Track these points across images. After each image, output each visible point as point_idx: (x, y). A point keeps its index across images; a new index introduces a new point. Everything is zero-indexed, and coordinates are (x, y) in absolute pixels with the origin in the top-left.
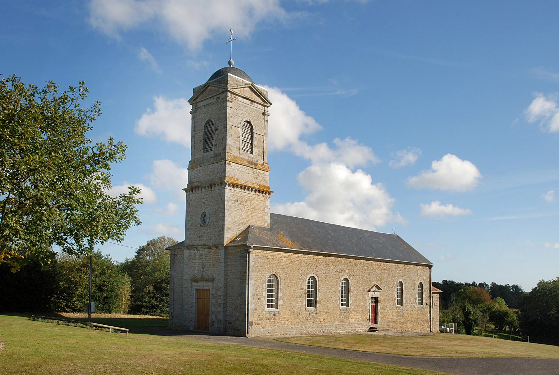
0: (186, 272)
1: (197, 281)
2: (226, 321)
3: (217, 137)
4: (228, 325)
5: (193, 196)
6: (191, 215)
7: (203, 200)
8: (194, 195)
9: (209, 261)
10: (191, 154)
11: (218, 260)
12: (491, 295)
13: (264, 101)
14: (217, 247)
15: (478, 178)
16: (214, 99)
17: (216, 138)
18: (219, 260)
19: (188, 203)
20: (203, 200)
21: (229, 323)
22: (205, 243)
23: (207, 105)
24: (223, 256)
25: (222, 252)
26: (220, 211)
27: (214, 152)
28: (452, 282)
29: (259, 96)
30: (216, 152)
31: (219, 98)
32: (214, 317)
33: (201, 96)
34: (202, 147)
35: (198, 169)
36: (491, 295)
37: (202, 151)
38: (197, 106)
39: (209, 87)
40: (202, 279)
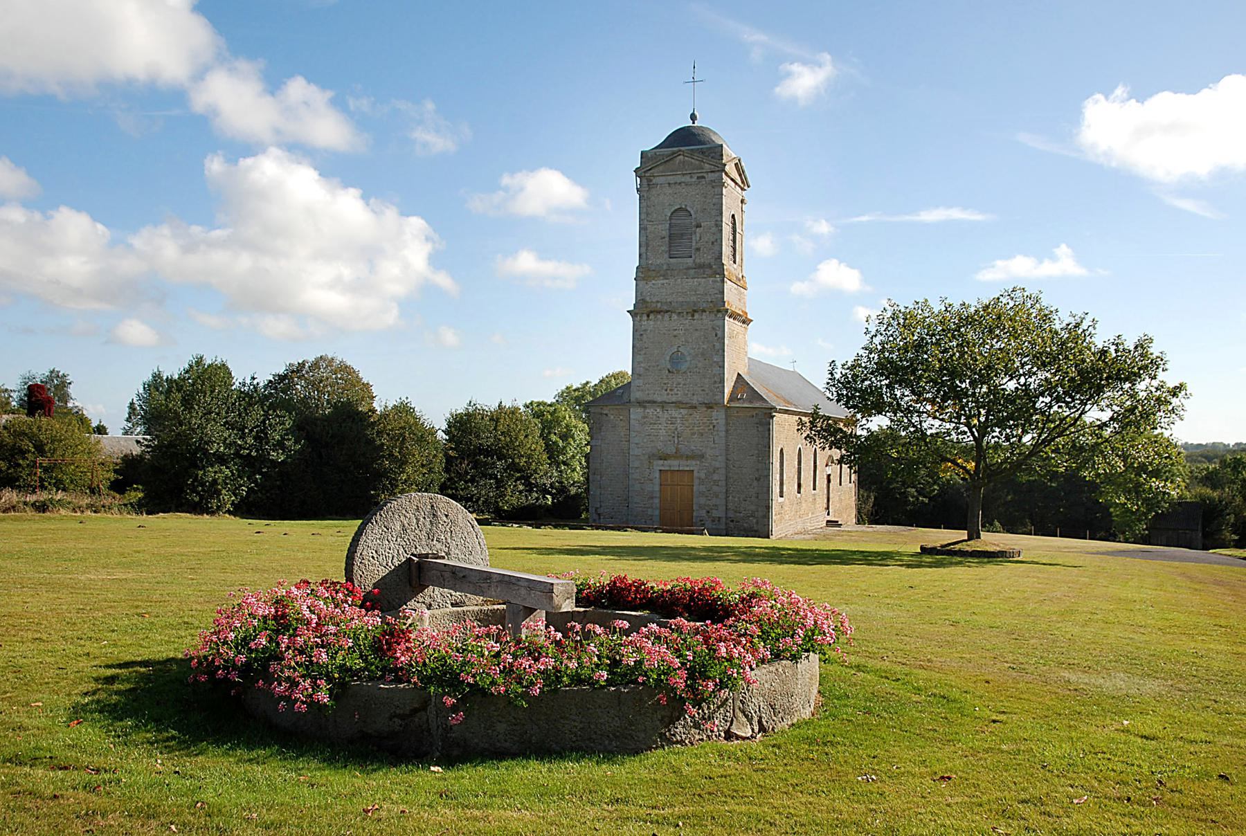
0: (637, 444)
1: (664, 457)
2: (727, 518)
3: (700, 238)
4: (732, 525)
5: (649, 324)
6: (645, 354)
7: (675, 333)
8: (651, 323)
9: (691, 428)
10: (640, 255)
11: (711, 427)
12: (1057, 251)
13: (743, 182)
14: (709, 406)
15: (1046, 318)
16: (691, 177)
17: (698, 239)
18: (714, 426)
19: (638, 333)
20: (675, 333)
21: (732, 521)
22: (680, 399)
23: (676, 183)
24: (722, 422)
25: (719, 416)
26: (714, 353)
27: (694, 261)
28: (1188, 93)
29: (740, 175)
30: (698, 261)
31: (704, 177)
32: (703, 513)
33: (661, 168)
34: (665, 248)
35: (662, 282)
36: (1057, 251)
37: (666, 255)
38: (651, 181)
39: (681, 157)
40: (678, 455)
